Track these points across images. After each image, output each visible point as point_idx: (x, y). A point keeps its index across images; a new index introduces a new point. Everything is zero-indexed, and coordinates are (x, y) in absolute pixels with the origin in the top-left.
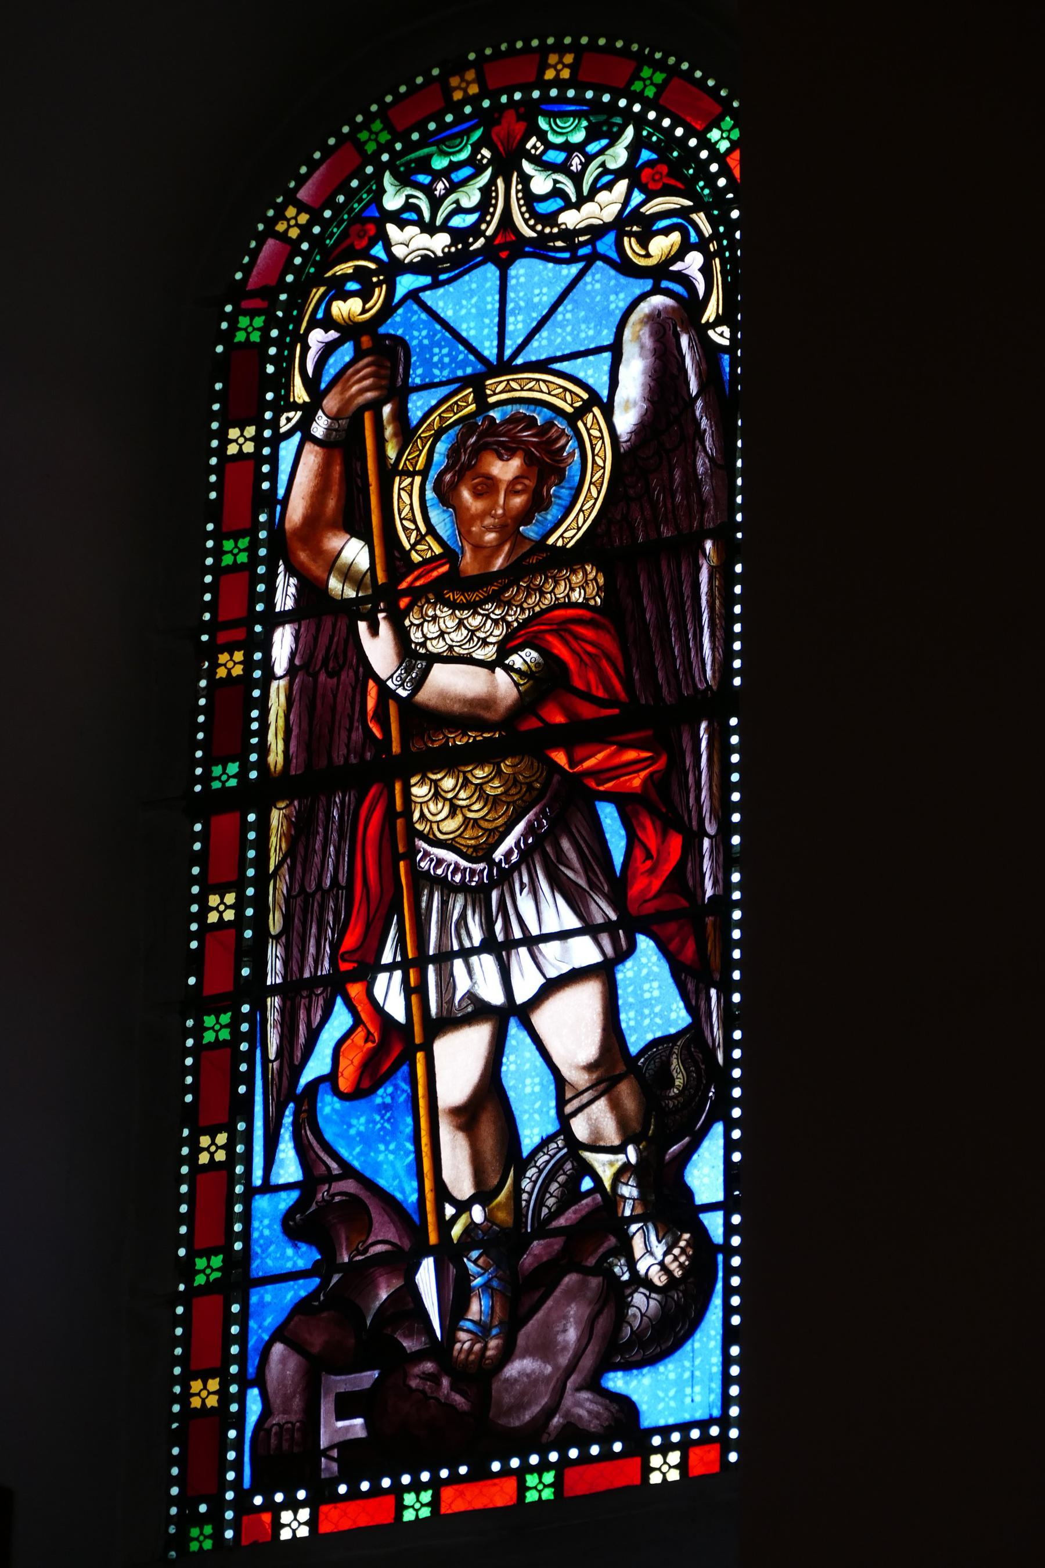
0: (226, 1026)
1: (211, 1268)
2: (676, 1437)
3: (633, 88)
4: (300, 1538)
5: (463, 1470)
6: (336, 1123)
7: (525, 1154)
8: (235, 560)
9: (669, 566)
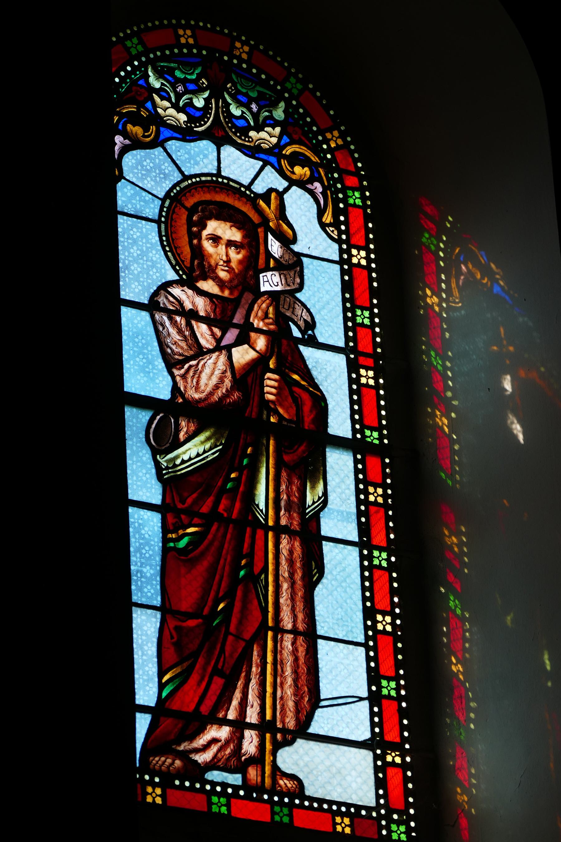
0: (380, 563)
1: (379, 557)
2: (361, 486)
3: (373, 384)
4: (156, 704)
5: (395, 585)
6: (335, 767)
7: (169, 289)
8: (384, 687)
9: (218, 530)
